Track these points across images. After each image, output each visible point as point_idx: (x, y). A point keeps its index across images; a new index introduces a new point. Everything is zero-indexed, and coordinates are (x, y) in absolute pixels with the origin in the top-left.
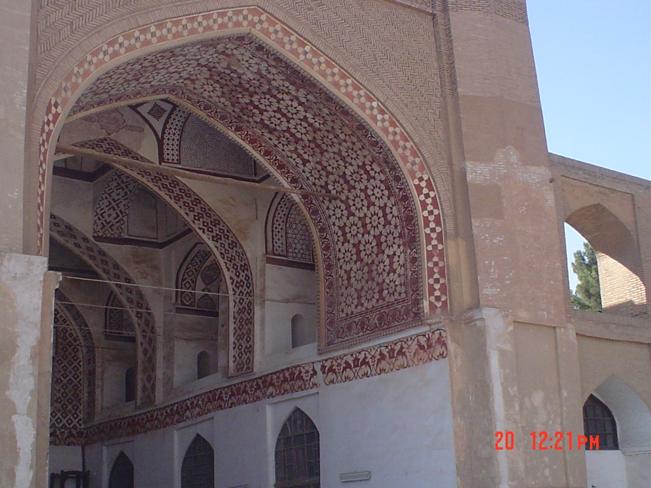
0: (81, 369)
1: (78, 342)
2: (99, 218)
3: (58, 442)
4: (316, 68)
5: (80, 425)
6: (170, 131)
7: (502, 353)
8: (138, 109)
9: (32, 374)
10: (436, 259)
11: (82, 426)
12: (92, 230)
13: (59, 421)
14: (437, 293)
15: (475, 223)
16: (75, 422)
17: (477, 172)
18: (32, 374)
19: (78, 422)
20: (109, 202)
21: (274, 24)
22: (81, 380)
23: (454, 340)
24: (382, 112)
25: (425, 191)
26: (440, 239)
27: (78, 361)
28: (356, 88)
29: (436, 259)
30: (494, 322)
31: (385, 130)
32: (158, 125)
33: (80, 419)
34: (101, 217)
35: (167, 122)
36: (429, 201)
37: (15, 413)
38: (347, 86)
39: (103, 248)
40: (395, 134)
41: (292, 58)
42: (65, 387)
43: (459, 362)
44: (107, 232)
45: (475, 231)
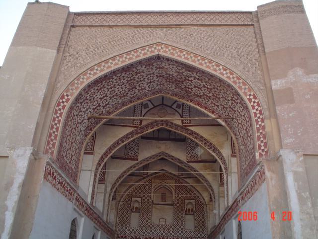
4: (190, 60)
7: (295, 173)
9: (17, 194)
10: (261, 131)
14: (263, 148)
15: (278, 108)
17: (277, 84)
18: (17, 194)
21: (168, 48)
23: (269, 170)
24: (225, 70)
25: (253, 100)
26: (263, 121)
28: (210, 63)
29: (261, 131)
30: (289, 158)
31: (228, 77)
32: (180, 111)
35: (183, 109)
36: (256, 104)
37: (7, 211)
38: (206, 63)
39: (192, 166)
40: (233, 78)
41: (179, 59)
43: (274, 182)
45: (278, 112)
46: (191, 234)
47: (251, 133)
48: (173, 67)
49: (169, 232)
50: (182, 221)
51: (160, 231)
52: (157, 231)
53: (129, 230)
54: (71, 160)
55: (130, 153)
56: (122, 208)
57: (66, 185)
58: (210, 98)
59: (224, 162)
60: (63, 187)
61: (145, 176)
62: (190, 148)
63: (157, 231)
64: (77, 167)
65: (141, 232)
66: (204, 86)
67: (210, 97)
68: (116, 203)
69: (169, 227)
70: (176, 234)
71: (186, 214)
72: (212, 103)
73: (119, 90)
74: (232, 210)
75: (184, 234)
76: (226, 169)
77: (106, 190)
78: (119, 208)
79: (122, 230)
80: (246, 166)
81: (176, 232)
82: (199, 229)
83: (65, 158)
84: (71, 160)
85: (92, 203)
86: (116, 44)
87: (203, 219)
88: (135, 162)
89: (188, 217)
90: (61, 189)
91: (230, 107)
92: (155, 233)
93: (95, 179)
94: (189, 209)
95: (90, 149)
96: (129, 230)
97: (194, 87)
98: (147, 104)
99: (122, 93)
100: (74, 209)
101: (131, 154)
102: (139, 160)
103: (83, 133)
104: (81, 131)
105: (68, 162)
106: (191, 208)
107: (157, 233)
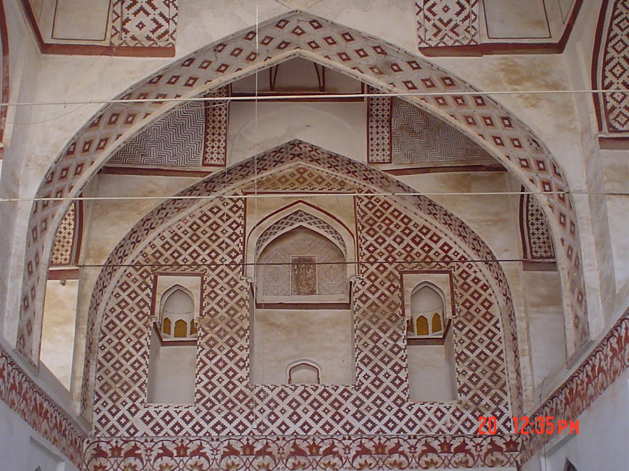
0: (500, 334)
1: (489, 291)
2: (426, 17)
3: (471, 462)
5: (509, 429)
11: (513, 431)
13: (468, 424)
19: (504, 424)
22: (502, 352)
27: (493, 321)
33: (508, 419)
42: (473, 366)
44: (446, 38)
46: (440, 424)
49: (337, 417)
50: (397, 369)
51: (295, 417)
53: (147, 418)
55: (135, 21)
57: (51, 410)
65: (207, 428)
69: (335, 395)
71: (410, 342)
78: (100, 322)
79: (113, 421)
81: (369, 416)
82: (476, 400)
87: (493, 356)
88: (154, 65)
89: (420, 352)
92: (273, 427)
94: (422, 319)
96: (147, 418)
100: (32, 439)
101: (141, 26)
102: (181, 53)
106: (429, 318)
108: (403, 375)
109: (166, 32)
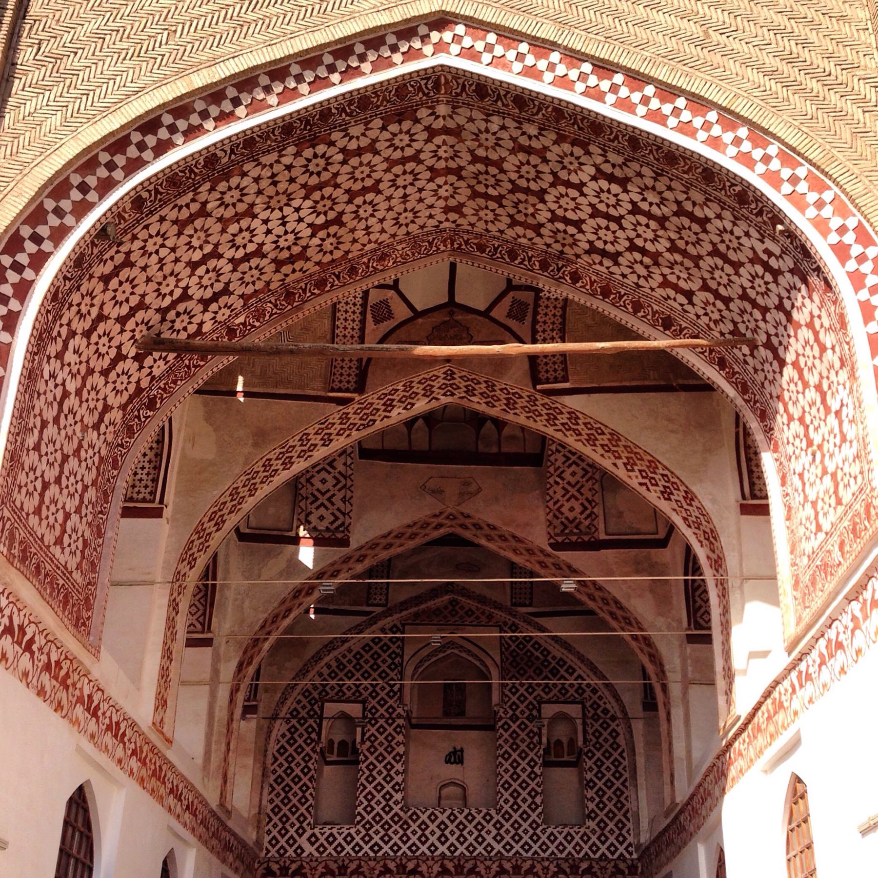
5: (631, 854)
6: (546, 335)
8: (492, 314)
12: (546, 537)
16: (621, 849)
20: (563, 488)
27: (620, 750)
33: (630, 845)
34: (557, 513)
35: (535, 322)
47: (843, 394)
48: (503, 127)
51: (462, 839)
52: (433, 839)
54: (64, 531)
56: (282, 750)
58: (657, 264)
59: (711, 538)
60: (28, 648)
61: (379, 610)
62: (561, 492)
63: (433, 839)
64: (91, 565)
66: (635, 210)
67: (655, 257)
68: (259, 728)
70: (508, 847)
71: (546, 764)
72: (665, 283)
73: (269, 232)
74: (759, 729)
75: (544, 847)
76: (718, 563)
77: (216, 672)
78: (273, 748)
80: (821, 536)
83: (33, 520)
84: (64, 531)
85: (158, 725)
86: (251, 16)
87: (618, 784)
90: (16, 658)
91: (744, 297)
93: (171, 624)
94: (559, 743)
95: (145, 493)
97: (592, 216)
98: (385, 302)
99: (282, 243)
103: (116, 415)
104: (107, 408)
105: (49, 539)
106: (565, 740)
107: (433, 848)
108: (538, 800)
109: (343, 524)
